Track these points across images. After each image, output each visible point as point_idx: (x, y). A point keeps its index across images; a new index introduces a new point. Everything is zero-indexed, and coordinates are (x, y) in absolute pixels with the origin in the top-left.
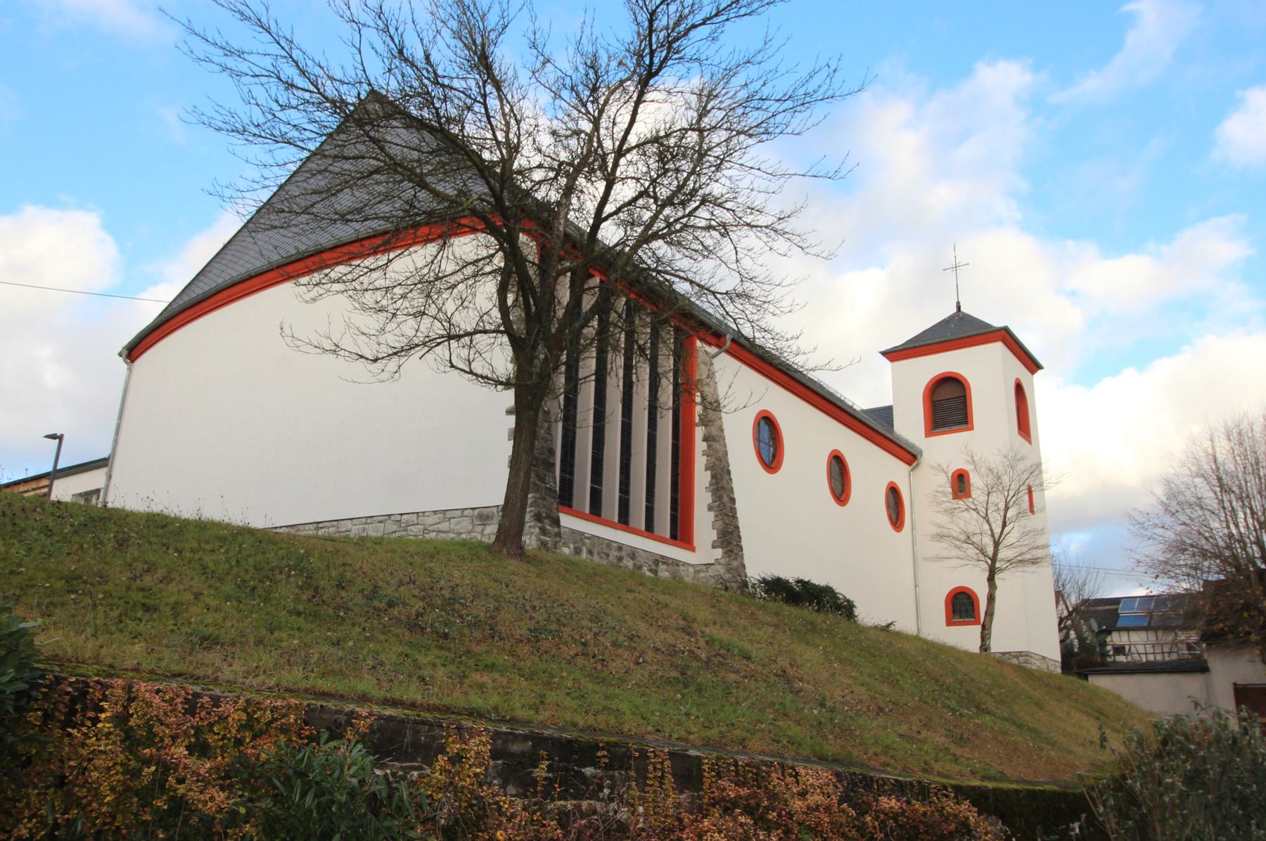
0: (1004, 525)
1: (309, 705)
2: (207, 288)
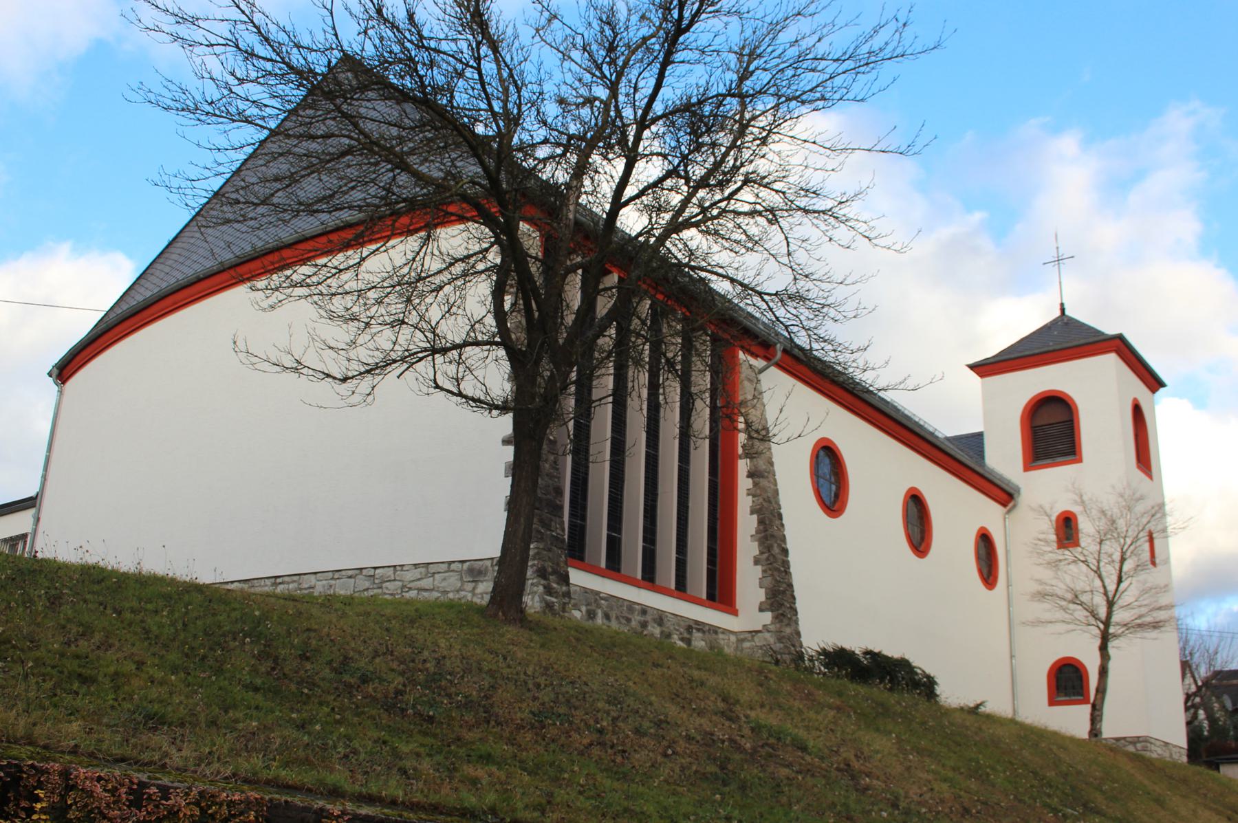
0: (1120, 580)
1: (271, 800)
2: (148, 294)
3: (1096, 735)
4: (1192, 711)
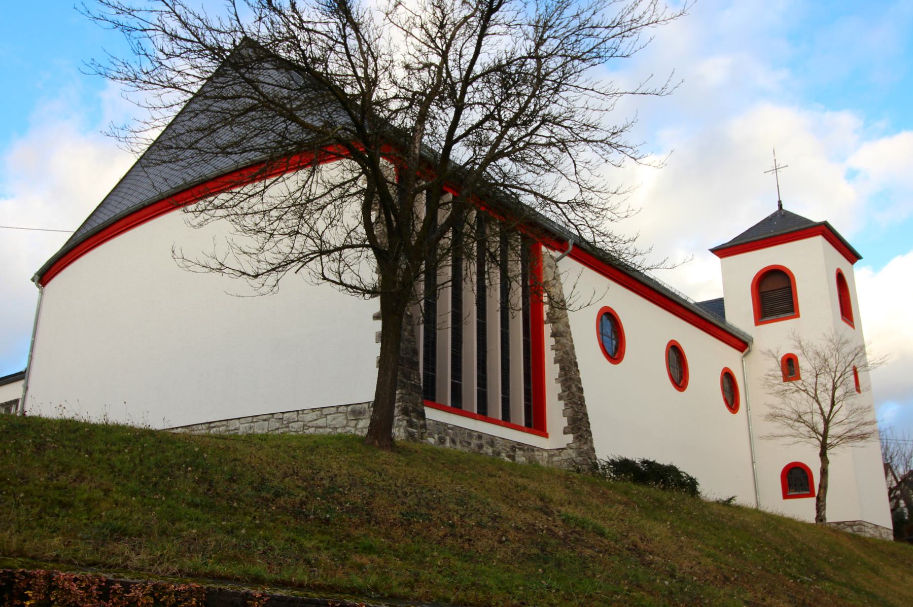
0: (833, 404)
1: (208, 589)
2: (106, 218)
3: (821, 521)
4: (895, 501)
